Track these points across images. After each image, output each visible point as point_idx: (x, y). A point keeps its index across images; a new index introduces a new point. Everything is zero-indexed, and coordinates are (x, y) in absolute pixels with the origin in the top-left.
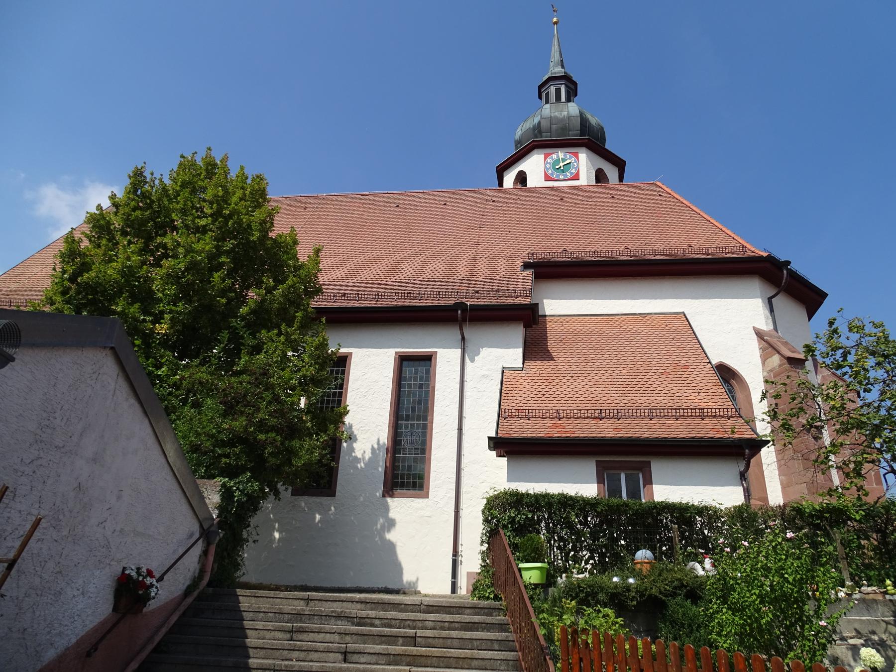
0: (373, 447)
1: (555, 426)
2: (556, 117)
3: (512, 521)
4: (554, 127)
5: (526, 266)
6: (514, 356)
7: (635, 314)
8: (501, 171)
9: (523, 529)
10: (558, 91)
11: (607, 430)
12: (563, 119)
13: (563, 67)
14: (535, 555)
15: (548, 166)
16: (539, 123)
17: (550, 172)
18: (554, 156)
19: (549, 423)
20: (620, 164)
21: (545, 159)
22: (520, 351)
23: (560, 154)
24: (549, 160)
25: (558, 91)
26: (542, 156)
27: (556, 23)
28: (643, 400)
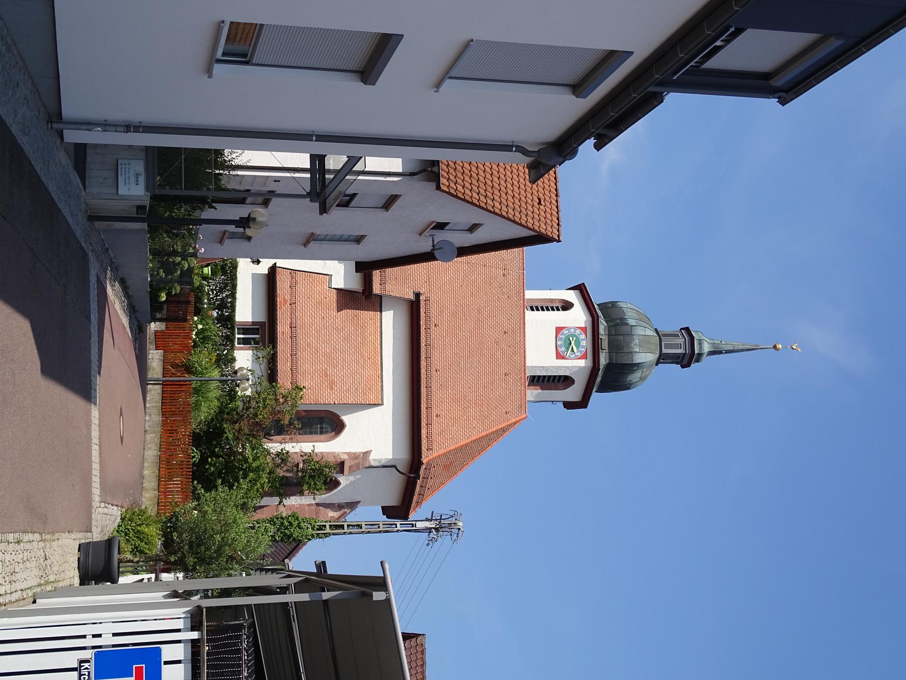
0: (598, 147)
1: (285, 301)
2: (633, 339)
3: (226, 265)
4: (621, 337)
5: (418, 295)
6: (339, 282)
7: (382, 371)
8: (581, 289)
9: (224, 272)
10: (678, 346)
11: (283, 328)
12: (629, 346)
13: (711, 353)
14: (214, 273)
15: (572, 330)
16: (627, 324)
17: (565, 332)
18: (583, 336)
19: (288, 297)
20: (583, 403)
21: (580, 328)
22: (341, 286)
23: (586, 342)
24: (578, 331)
25: (678, 346)
26: (583, 326)
27: (775, 347)
28: (304, 356)
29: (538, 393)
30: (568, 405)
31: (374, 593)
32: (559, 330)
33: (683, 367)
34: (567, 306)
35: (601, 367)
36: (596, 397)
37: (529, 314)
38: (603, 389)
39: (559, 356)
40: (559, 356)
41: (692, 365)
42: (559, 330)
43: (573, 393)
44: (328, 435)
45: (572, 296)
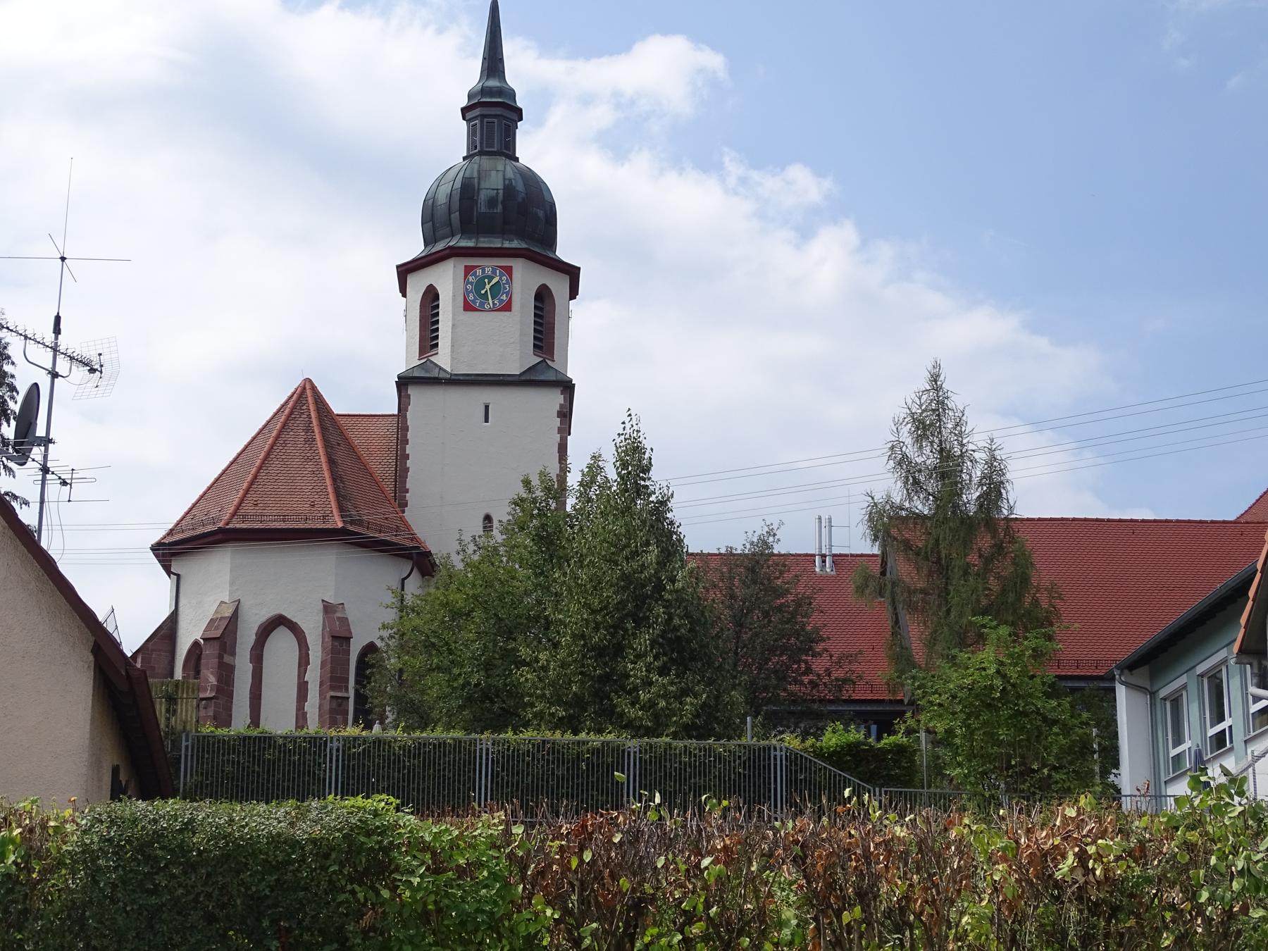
15: (469, 287)
20: (572, 273)
23: (488, 265)
24: (471, 279)
29: (548, 45)
30: (574, 293)
31: (38, 434)
32: (468, 307)
33: (521, 119)
34: (431, 297)
35: (524, 246)
36: (564, 252)
37: (444, 359)
38: (549, 238)
39: (507, 307)
40: (507, 307)
41: (519, 104)
42: (468, 307)
43: (559, 286)
44: (442, 198)
45: (418, 284)
